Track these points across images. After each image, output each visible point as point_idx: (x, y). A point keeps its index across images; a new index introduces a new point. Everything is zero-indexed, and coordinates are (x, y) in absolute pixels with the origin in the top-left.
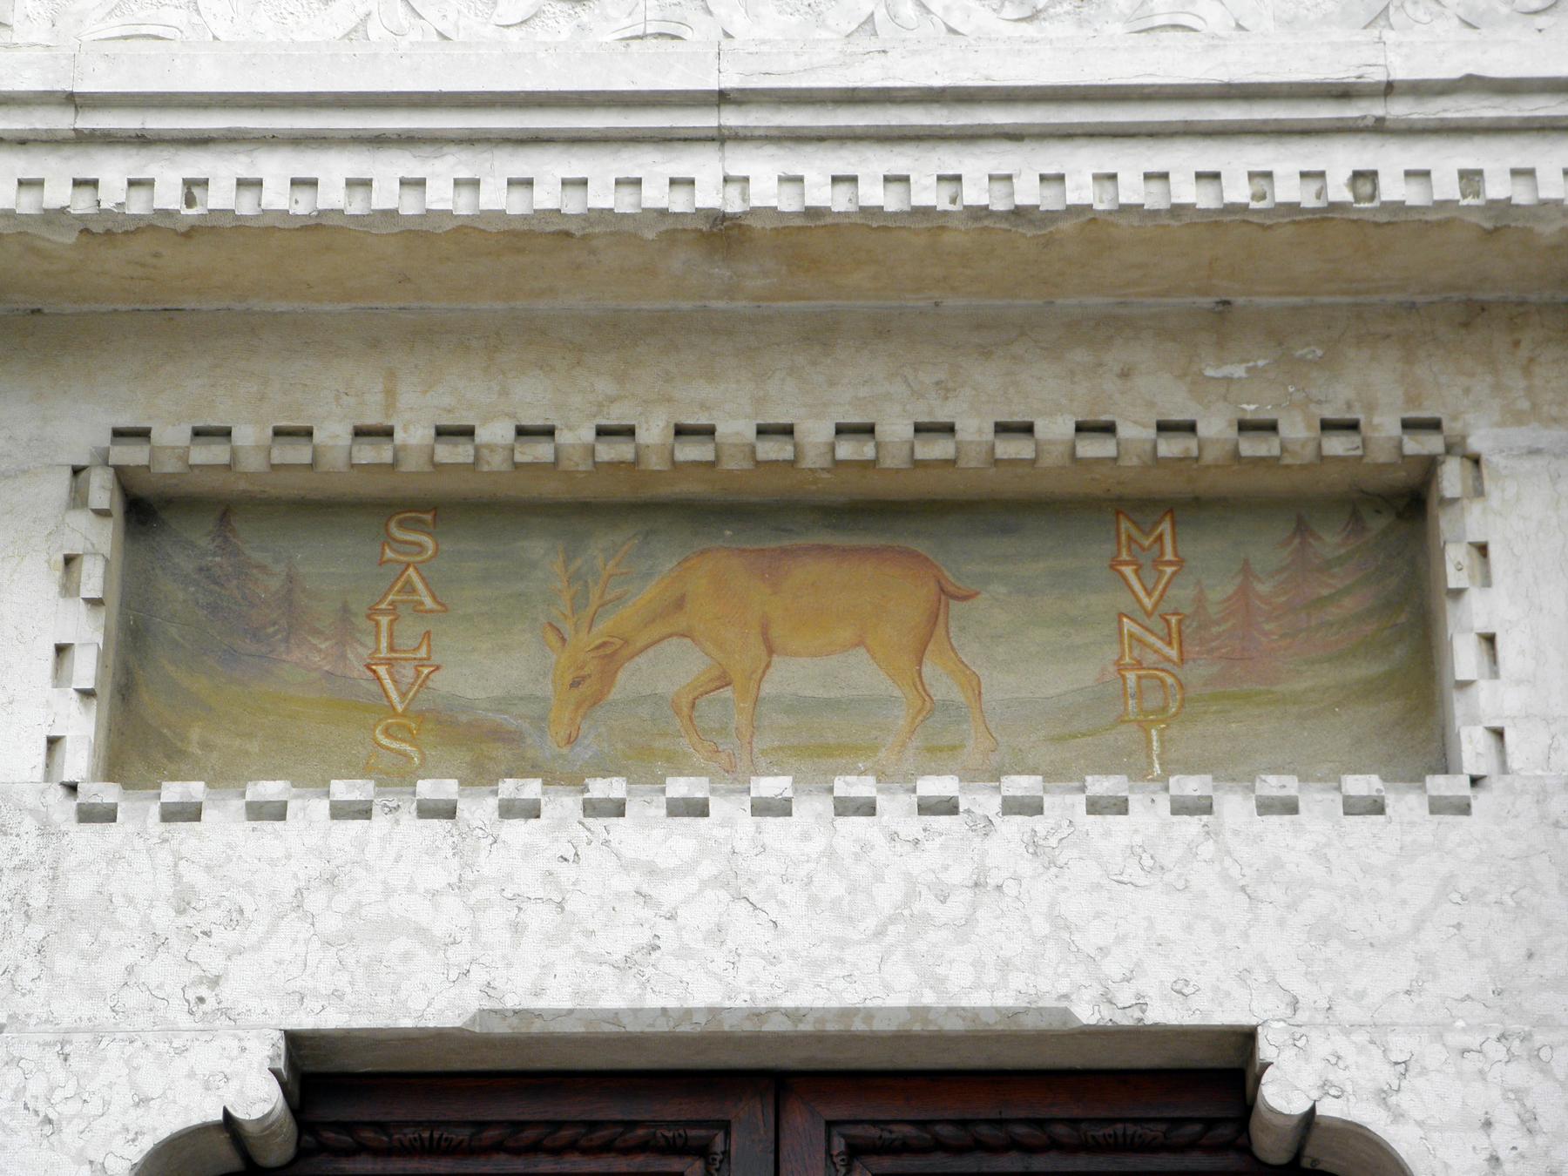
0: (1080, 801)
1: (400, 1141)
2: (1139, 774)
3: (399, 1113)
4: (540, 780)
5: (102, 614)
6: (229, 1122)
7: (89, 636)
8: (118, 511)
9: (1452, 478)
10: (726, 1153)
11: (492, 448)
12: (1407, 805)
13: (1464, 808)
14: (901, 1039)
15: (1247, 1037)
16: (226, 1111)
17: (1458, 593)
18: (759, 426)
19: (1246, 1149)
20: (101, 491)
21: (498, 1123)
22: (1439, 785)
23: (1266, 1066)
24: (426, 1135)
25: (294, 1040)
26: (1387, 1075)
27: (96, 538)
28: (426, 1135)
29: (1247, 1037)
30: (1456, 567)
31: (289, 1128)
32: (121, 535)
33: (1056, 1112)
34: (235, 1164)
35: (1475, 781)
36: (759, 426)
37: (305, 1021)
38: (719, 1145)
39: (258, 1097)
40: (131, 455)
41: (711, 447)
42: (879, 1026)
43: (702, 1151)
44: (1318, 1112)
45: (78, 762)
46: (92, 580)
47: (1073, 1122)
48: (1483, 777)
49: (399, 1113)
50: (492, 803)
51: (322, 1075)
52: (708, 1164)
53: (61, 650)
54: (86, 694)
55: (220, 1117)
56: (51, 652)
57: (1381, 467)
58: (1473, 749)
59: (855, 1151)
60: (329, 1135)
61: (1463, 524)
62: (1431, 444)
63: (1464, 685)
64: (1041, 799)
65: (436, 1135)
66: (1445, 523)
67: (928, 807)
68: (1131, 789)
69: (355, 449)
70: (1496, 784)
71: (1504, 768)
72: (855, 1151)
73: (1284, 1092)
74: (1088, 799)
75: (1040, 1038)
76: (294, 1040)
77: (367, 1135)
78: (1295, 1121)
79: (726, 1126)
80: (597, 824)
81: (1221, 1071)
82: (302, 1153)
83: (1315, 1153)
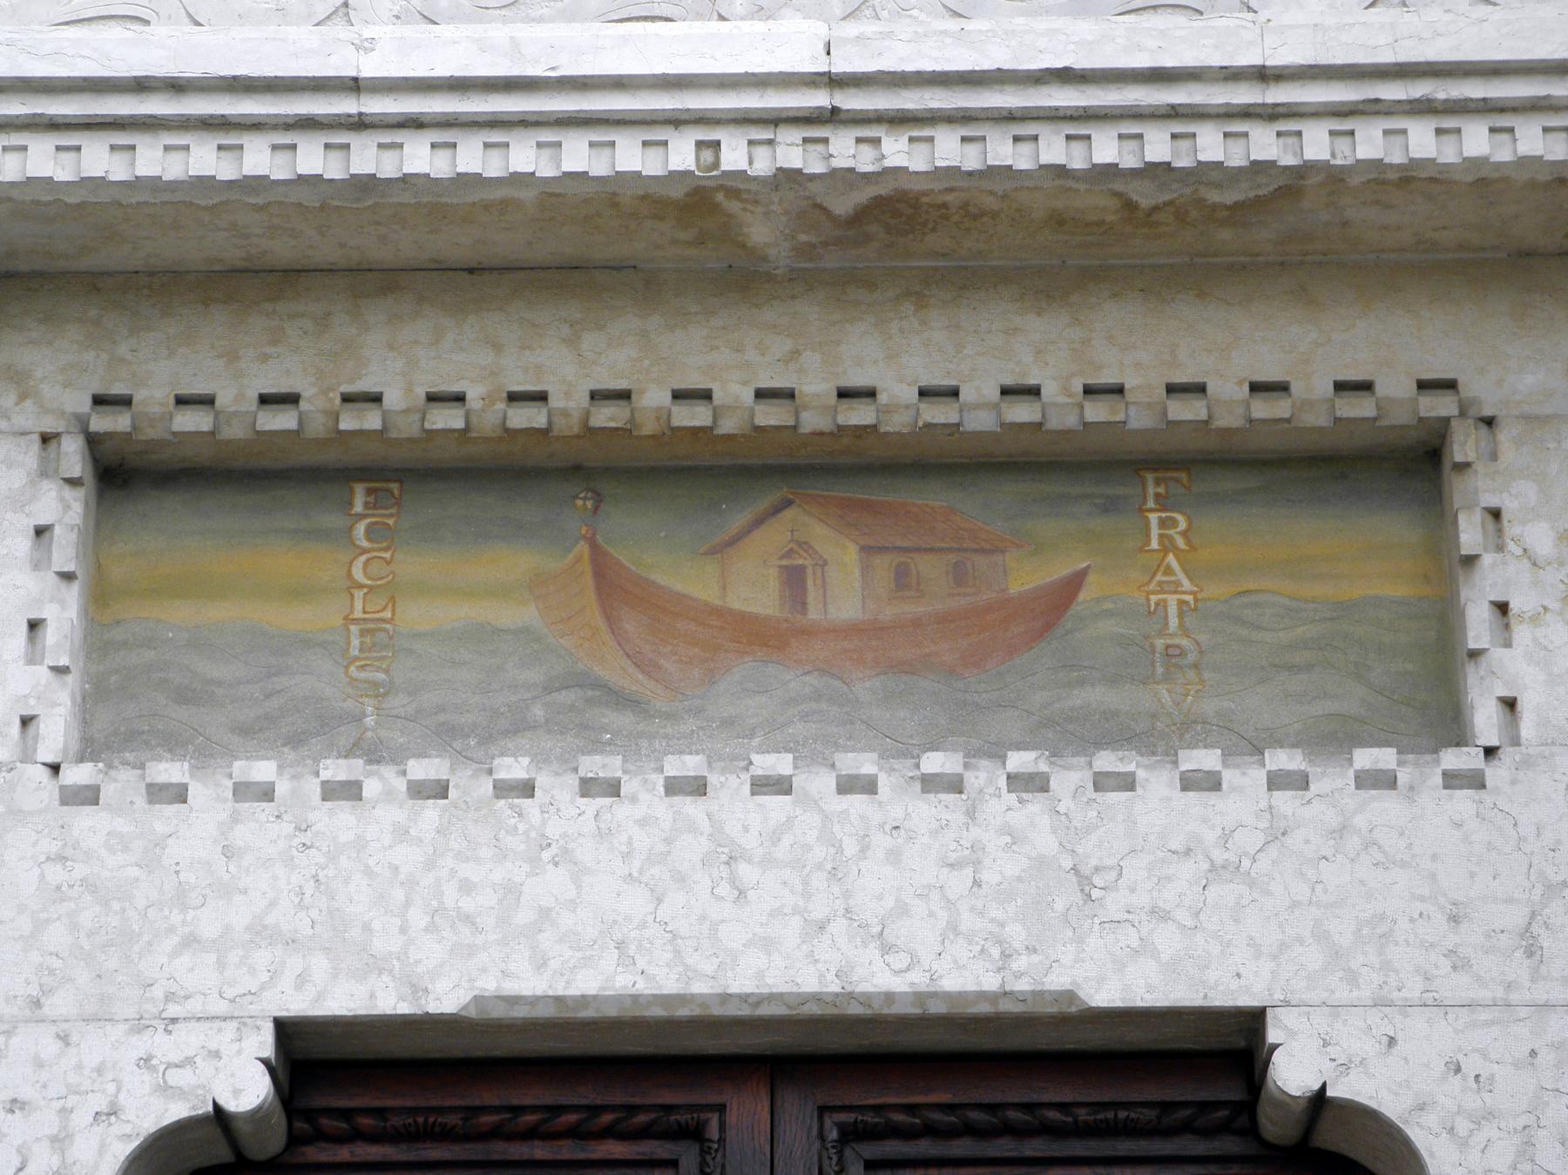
0: (572, 781)
1: (678, 1123)
2: (374, 754)
3: (490, 1097)
4: (1219, 752)
6: (219, 1115)
7: (64, 614)
8: (89, 480)
9: (1464, 445)
10: (722, 1140)
11: (565, 413)
12: (1423, 776)
13: (1476, 781)
14: (904, 1022)
15: (1254, 1020)
16: (215, 1104)
18: (1085, 386)
21: (497, 1109)
22: (1453, 759)
23: (1275, 1047)
24: (421, 1120)
25: (286, 1030)
27: (64, 508)
28: (421, 1120)
29: (1254, 1020)
31: (279, 1119)
32: (93, 504)
33: (1047, 1097)
34: (223, 1154)
35: (1490, 752)
36: (1085, 386)
37: (299, 1005)
38: (713, 1132)
39: (246, 1087)
40: (102, 423)
41: (544, 411)
42: (897, 1009)
43: (695, 1133)
44: (1330, 1093)
46: (65, 553)
48: (1497, 748)
49: (490, 1097)
50: (1260, 776)
51: (311, 1059)
52: (704, 1152)
55: (210, 1108)
56: (25, 627)
57: (1227, 432)
58: (1486, 722)
59: (849, 1134)
60: (325, 1122)
61: (1477, 490)
63: (1474, 654)
64: (273, 784)
65: (431, 1120)
67: (503, 789)
68: (1225, 764)
69: (260, 414)
70: (1508, 755)
71: (1516, 741)
72: (849, 1134)
73: (1293, 1072)
74: (409, 782)
75: (1062, 1021)
76: (286, 1030)
77: (976, 1116)
78: (1303, 1104)
79: (721, 1109)
80: (592, 805)
81: (1228, 1048)
82: (294, 1140)
83: (1329, 1137)
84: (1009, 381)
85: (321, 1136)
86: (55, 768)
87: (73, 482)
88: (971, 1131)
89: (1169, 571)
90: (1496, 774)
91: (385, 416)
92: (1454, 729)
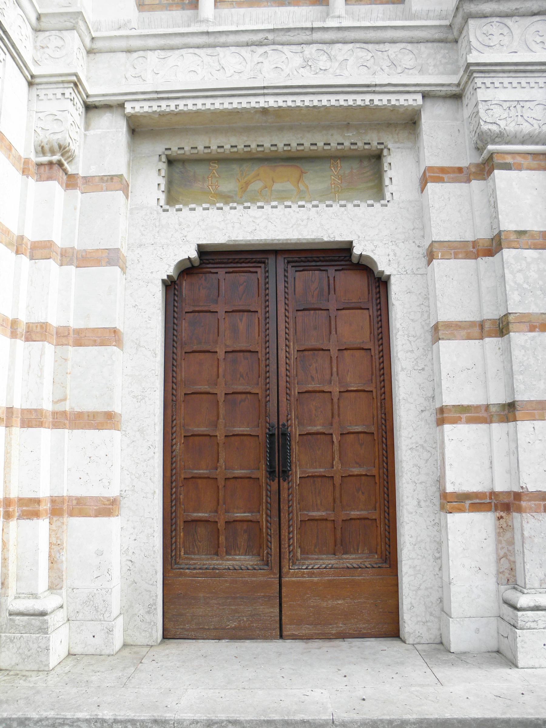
6: (189, 258)
8: (167, 162)
9: (385, 152)
11: (227, 149)
12: (377, 205)
15: (351, 242)
19: (351, 261)
20: (164, 159)
22: (383, 202)
25: (199, 246)
27: (163, 166)
31: (198, 259)
35: (388, 201)
39: (193, 254)
45: (162, 202)
46: (163, 173)
58: (388, 196)
60: (205, 261)
61: (386, 160)
62: (382, 147)
66: (384, 159)
70: (391, 202)
73: (357, 251)
76: (199, 246)
77: (315, 258)
82: (201, 264)
84: (299, 143)
85: (204, 263)
86: (162, 207)
87: (164, 162)
88: (321, 261)
89: (214, 173)
90: (389, 204)
91: (172, 152)
92: (383, 198)
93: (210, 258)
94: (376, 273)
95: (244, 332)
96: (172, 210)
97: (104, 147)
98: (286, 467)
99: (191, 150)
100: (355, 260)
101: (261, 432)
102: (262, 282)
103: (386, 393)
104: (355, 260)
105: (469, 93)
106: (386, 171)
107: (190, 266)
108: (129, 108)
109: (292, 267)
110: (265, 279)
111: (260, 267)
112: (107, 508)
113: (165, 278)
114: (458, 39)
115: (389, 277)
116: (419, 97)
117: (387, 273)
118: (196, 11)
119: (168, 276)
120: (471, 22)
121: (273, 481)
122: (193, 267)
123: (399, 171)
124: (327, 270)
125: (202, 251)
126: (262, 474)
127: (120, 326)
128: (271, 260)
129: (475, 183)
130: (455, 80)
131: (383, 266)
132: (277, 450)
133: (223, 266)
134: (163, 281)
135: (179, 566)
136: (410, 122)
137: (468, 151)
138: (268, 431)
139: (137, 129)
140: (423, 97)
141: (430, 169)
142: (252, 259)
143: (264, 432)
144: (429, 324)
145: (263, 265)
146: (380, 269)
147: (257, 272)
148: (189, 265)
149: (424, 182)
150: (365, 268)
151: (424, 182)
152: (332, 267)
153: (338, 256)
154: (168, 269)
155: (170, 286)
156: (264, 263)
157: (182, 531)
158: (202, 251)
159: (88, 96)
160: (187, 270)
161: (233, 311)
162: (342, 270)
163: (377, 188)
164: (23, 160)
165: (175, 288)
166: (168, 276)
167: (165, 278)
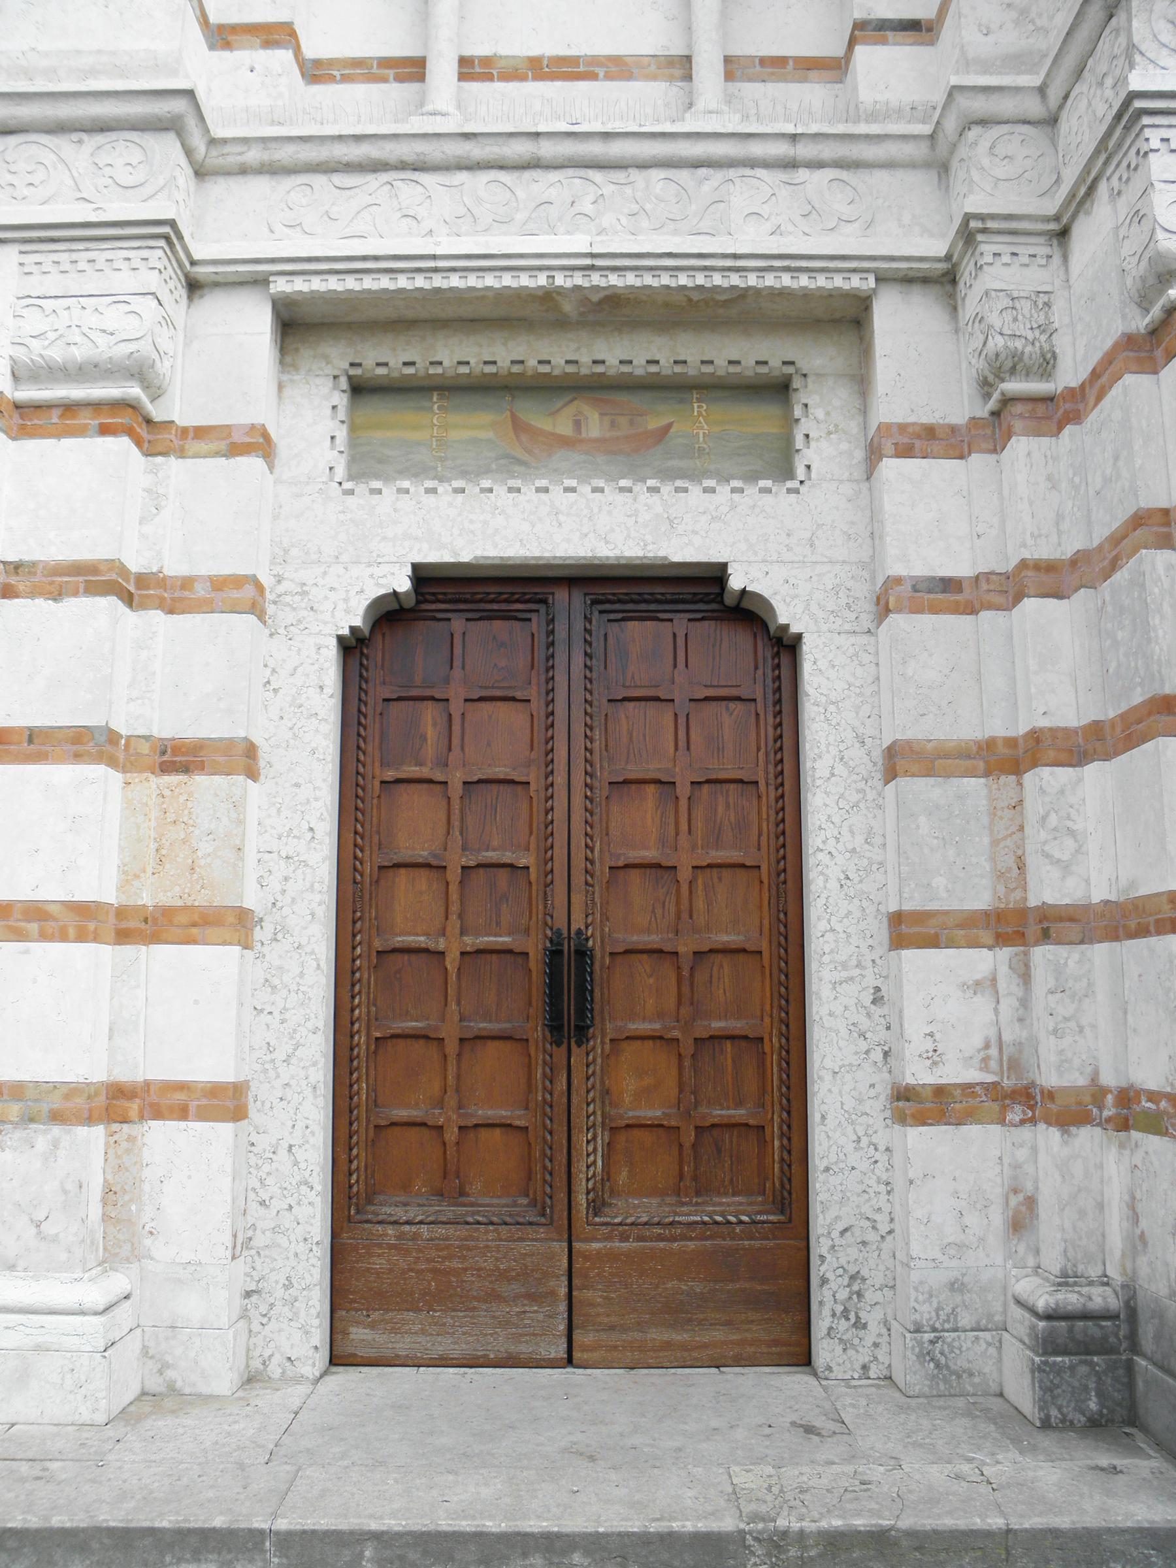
5: (345, 426)
6: (395, 593)
7: (342, 434)
9: (796, 383)
12: (780, 489)
15: (724, 566)
17: (797, 420)
19: (722, 602)
20: (344, 383)
22: (790, 484)
25: (415, 567)
26: (293, 994)
27: (341, 400)
30: (798, 412)
31: (413, 595)
35: (802, 482)
39: (403, 584)
40: (354, 372)
45: (340, 472)
46: (342, 414)
47: (662, 594)
53: (334, 407)
54: (343, 422)
58: (801, 473)
62: (790, 370)
66: (794, 397)
70: (807, 483)
73: (736, 583)
76: (415, 567)
79: (553, 594)
82: (418, 602)
86: (340, 483)
87: (343, 391)
90: (803, 489)
93: (442, 595)
94: (772, 630)
95: (500, 741)
96: (361, 489)
97: (226, 360)
98: (584, 1021)
99: (403, 358)
100: (729, 601)
101: (535, 947)
102: (541, 639)
103: (789, 871)
104: (729, 601)
105: (967, 273)
106: (796, 390)
107: (396, 607)
108: (280, 286)
109: (601, 612)
110: (548, 648)
111: (538, 611)
112: (226, 1102)
113: (346, 632)
114: (948, 161)
115: (799, 637)
116: (872, 283)
117: (794, 629)
118: (414, 86)
119: (352, 629)
120: (974, 133)
121: (558, 1045)
122: (402, 610)
123: (825, 431)
124: (671, 620)
125: (423, 576)
126: (537, 1032)
127: (257, 740)
128: (560, 596)
129: (977, 460)
130: (938, 248)
131: (788, 614)
132: (568, 988)
133: (462, 606)
134: (340, 639)
135: (365, 1217)
136: (849, 319)
137: (965, 387)
138: (548, 945)
139: (295, 326)
140: (877, 280)
141: (884, 429)
142: (525, 594)
143: (540, 947)
144: (881, 745)
145: (542, 608)
146: (782, 620)
147: (530, 620)
148: (396, 606)
149: (874, 455)
150: (748, 614)
151: (874, 455)
152: (682, 615)
153: (701, 594)
154: (354, 617)
155: (352, 648)
156: (544, 601)
157: (376, 1156)
158: (423, 576)
159: (193, 263)
160: (389, 615)
161: (481, 699)
162: (703, 619)
163: (780, 463)
164: (132, 576)
165: (362, 653)
166: (352, 629)
167: (346, 632)
